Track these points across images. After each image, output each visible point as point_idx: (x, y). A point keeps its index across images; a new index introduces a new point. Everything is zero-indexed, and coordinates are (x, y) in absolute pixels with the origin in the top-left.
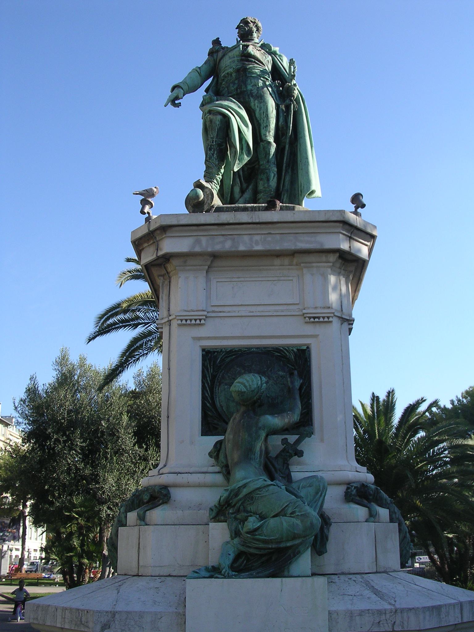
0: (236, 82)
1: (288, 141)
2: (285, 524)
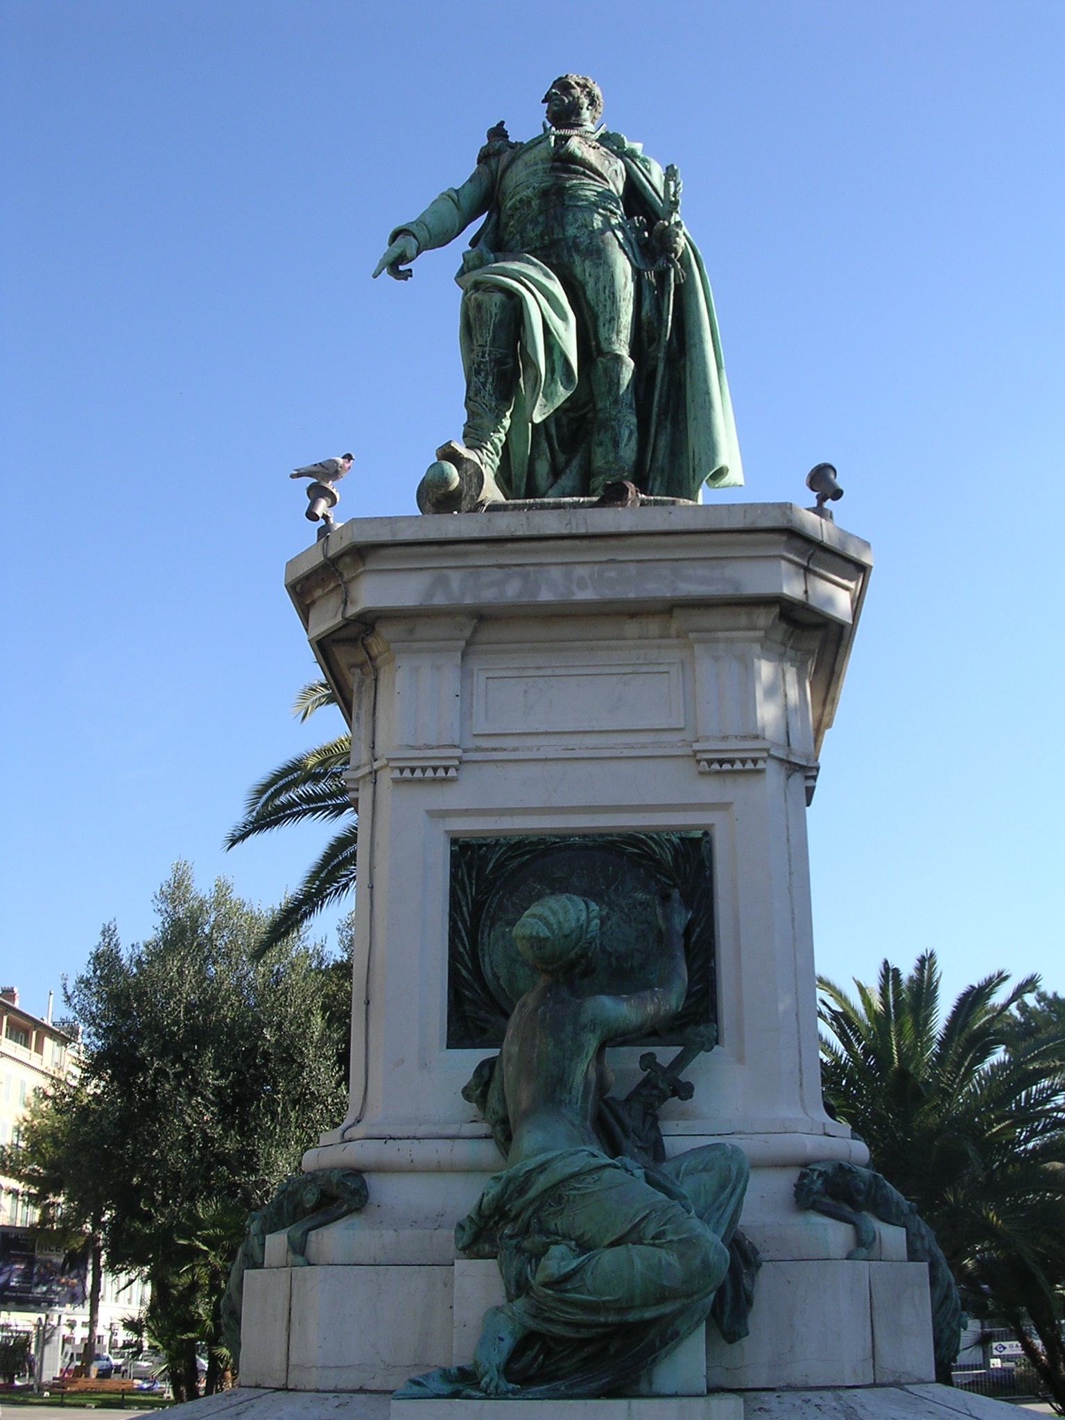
0: (541, 219)
1: (661, 355)
2: (639, 1265)
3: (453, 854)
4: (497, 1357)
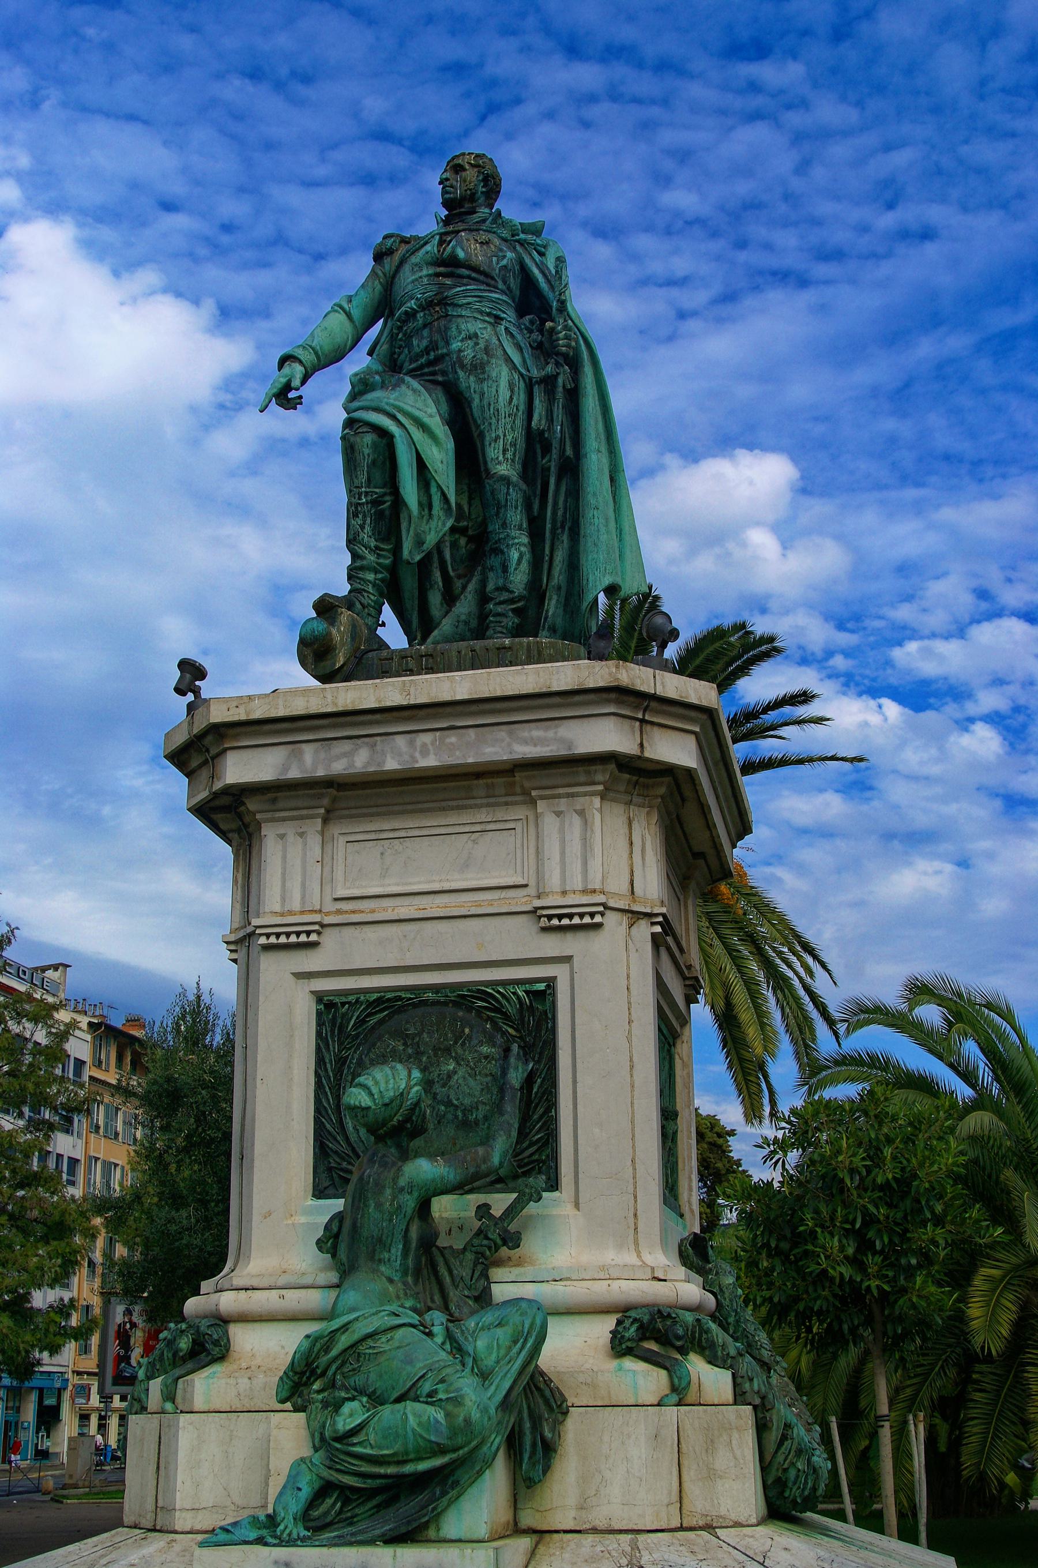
2: (412, 1421)
3: (319, 1014)
4: (295, 1505)
